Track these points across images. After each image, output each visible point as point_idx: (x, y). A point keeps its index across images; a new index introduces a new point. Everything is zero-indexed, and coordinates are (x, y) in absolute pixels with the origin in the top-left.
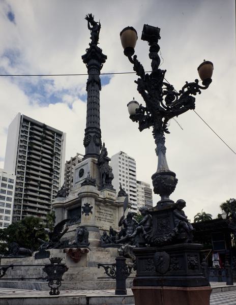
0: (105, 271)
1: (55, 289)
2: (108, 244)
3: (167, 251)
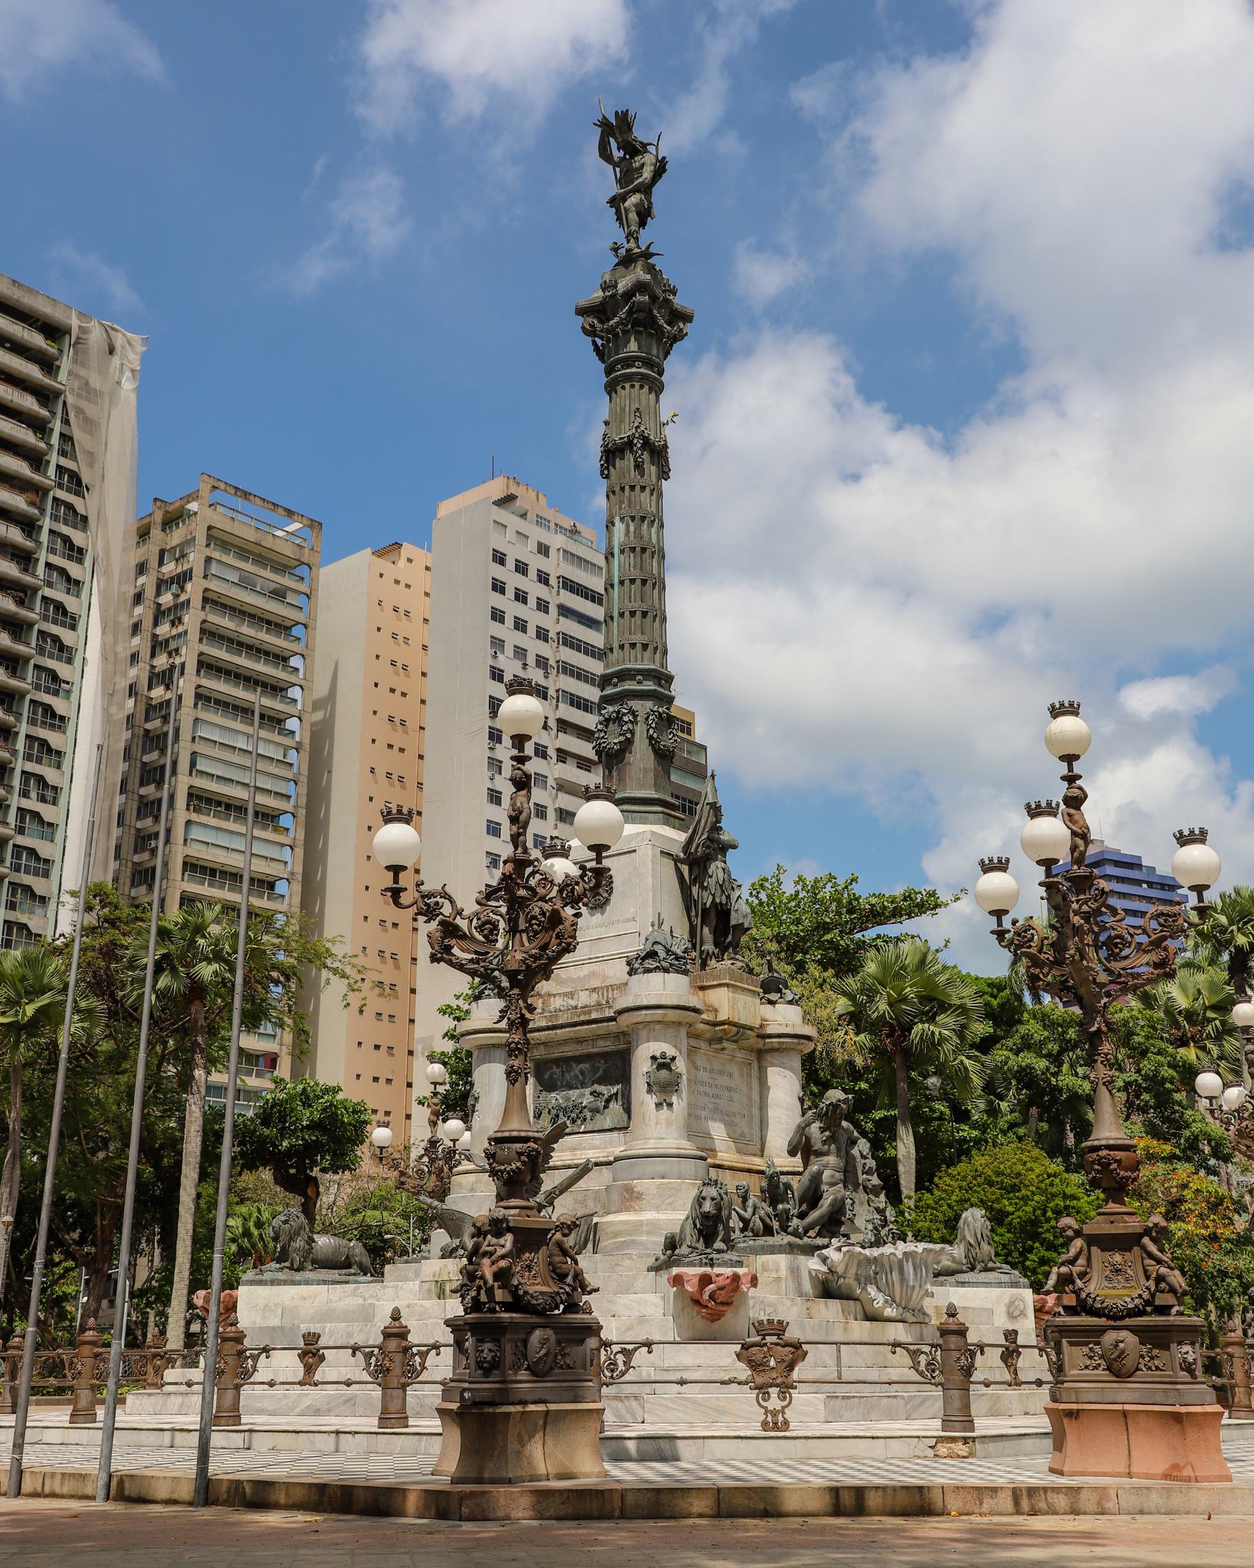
0: (910, 1363)
1: (774, 1413)
2: (761, 1241)
3: (1133, 1330)
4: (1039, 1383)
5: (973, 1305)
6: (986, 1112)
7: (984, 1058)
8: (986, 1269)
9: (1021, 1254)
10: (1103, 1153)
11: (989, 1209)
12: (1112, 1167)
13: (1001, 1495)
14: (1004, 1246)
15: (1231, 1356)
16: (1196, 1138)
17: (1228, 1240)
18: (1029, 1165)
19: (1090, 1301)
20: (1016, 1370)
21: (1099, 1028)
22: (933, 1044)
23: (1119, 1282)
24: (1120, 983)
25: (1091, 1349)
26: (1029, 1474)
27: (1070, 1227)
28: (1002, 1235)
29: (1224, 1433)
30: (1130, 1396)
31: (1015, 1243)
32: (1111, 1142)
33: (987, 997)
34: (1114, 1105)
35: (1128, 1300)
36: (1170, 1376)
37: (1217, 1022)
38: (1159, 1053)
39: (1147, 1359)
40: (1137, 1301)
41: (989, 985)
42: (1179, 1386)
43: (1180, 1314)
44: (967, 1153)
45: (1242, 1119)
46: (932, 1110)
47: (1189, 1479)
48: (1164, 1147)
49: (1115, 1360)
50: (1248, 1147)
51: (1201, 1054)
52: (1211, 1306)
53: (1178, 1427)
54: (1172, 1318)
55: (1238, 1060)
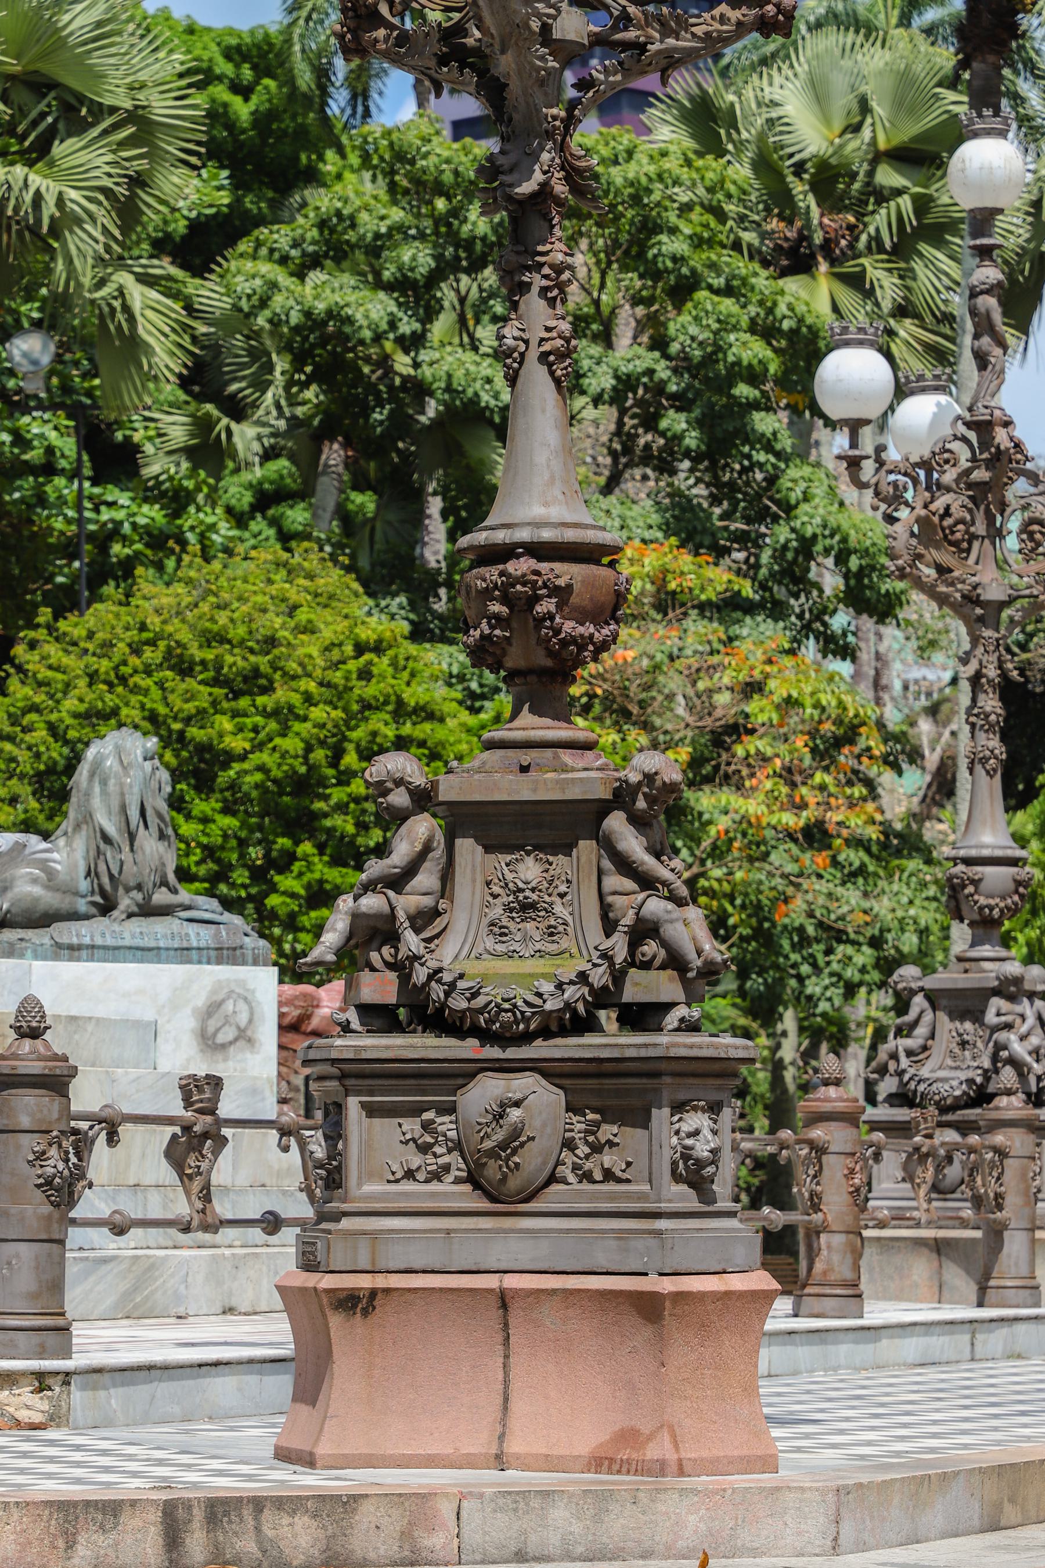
4: (272, 1223)
5: (100, 1012)
6: (189, 452)
7: (193, 286)
8: (147, 911)
9: (259, 874)
10: (521, 566)
11: (175, 741)
12: (541, 609)
13: (130, 1521)
14: (210, 852)
15: (819, 1150)
16: (806, 546)
17: (858, 843)
18: (303, 615)
19: (437, 991)
20: (207, 1187)
21: (545, 186)
22: (34, 230)
23: (526, 939)
24: (626, 45)
25: (426, 1126)
26: (216, 1464)
27: (399, 782)
28: (205, 820)
29: (767, 1356)
30: (522, 1253)
31: (242, 843)
32: (547, 535)
33: (221, 92)
34: (569, 450)
35: (547, 987)
36: (642, 1197)
37: (905, 203)
38: (728, 291)
39: (583, 1150)
40: (570, 992)
41: (228, 54)
42: (662, 1224)
43: (691, 1027)
44: (126, 569)
45: (935, 488)
46: (20, 440)
47: (660, 1468)
48: (711, 572)
49: (492, 1154)
50: (942, 570)
51: (847, 298)
52: (789, 1021)
53: (647, 1331)
54: (663, 1039)
55: (949, 318)
